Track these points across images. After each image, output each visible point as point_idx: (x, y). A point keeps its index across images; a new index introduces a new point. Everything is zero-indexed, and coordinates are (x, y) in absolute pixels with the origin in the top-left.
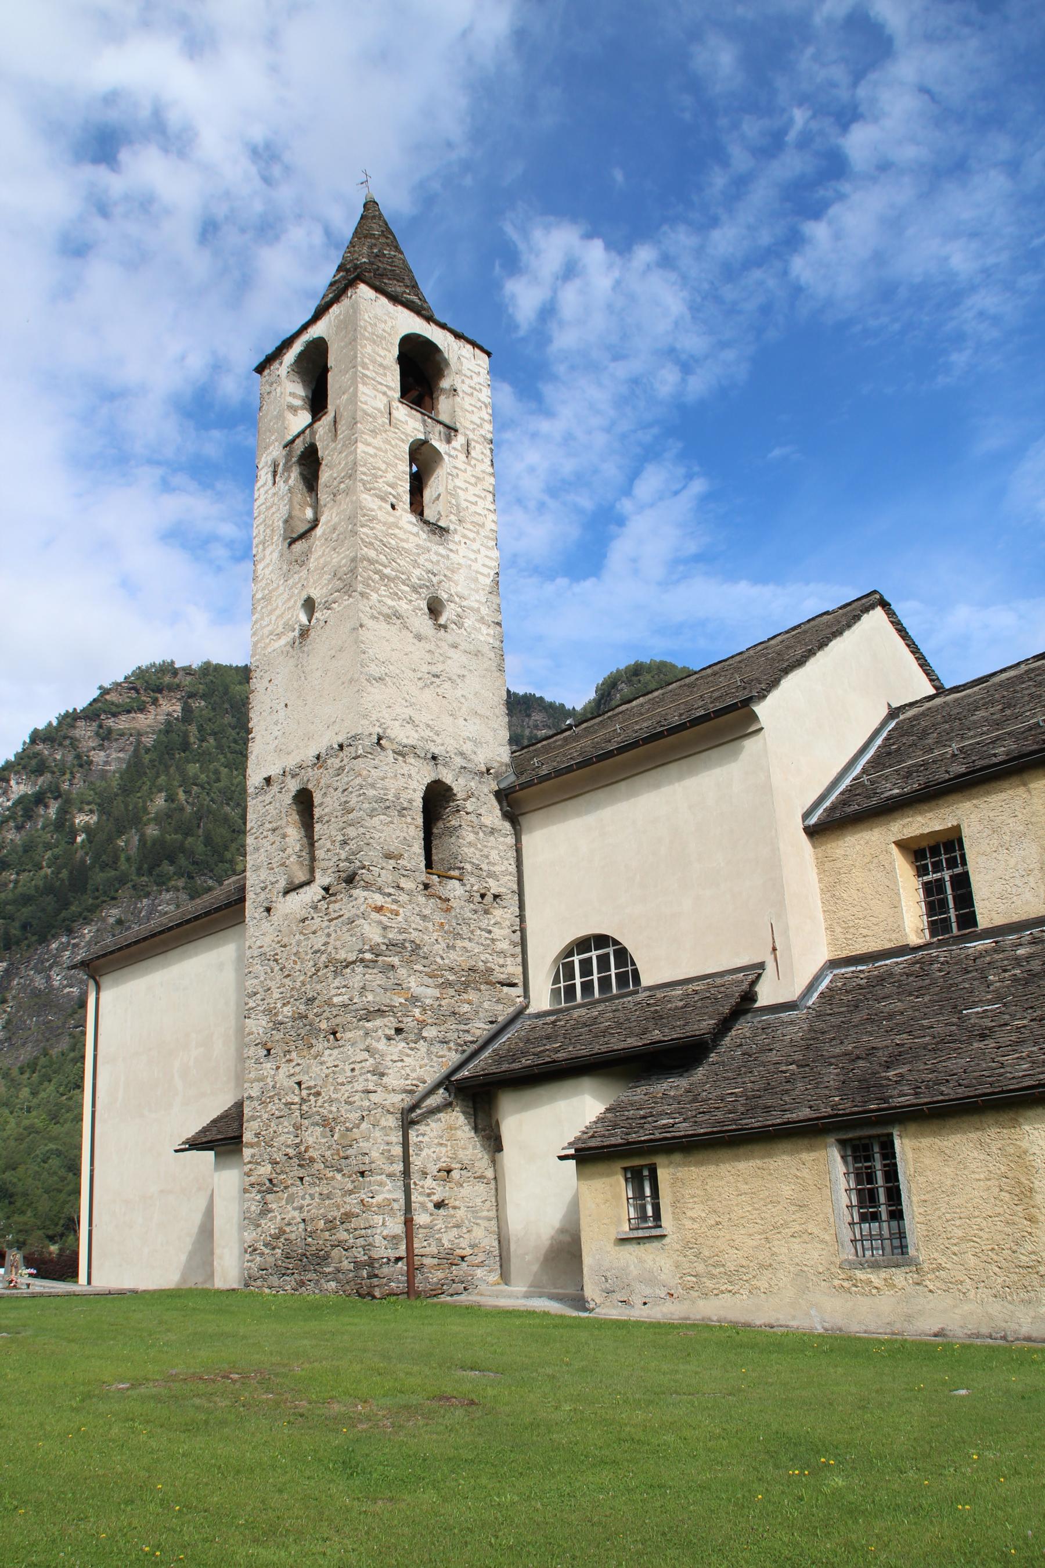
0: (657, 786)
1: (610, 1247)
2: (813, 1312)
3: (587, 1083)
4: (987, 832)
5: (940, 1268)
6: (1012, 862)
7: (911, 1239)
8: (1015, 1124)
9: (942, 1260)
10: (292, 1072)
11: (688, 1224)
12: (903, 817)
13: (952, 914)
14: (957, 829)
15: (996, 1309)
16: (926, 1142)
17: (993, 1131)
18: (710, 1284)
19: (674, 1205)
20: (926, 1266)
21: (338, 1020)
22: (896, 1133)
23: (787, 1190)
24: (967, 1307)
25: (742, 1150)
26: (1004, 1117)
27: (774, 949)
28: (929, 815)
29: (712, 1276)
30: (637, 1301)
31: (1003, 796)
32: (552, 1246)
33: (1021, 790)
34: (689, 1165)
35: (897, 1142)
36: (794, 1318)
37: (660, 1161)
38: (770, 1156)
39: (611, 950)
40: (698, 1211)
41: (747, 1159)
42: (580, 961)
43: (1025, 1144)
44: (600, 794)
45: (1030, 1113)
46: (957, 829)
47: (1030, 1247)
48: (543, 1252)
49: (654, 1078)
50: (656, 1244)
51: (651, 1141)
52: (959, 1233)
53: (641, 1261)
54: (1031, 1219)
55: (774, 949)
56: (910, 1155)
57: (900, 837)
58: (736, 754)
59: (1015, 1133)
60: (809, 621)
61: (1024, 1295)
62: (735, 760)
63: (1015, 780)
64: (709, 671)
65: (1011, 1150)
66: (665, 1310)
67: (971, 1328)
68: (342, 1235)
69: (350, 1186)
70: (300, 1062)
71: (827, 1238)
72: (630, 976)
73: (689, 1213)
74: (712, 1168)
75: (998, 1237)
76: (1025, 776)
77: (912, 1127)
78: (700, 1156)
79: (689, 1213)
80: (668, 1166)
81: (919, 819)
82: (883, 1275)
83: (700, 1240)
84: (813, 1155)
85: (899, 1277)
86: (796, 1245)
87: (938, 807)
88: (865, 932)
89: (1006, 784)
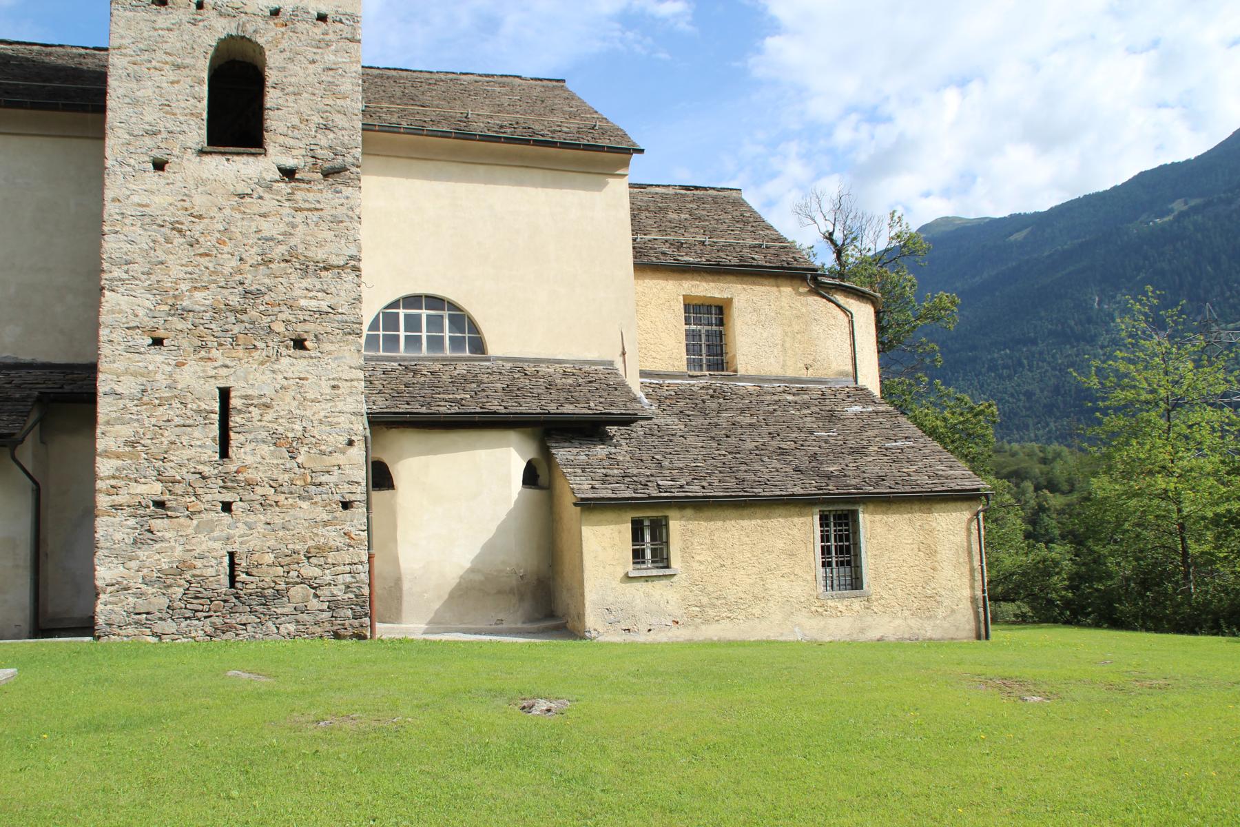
0: (521, 183)
1: (616, 584)
2: (796, 629)
3: (513, 436)
4: (750, 309)
5: (882, 598)
6: (765, 335)
7: (866, 579)
8: (930, 512)
9: (883, 593)
10: (213, 373)
11: (695, 565)
12: (692, 279)
13: (424, 334)
14: (729, 301)
15: (913, 622)
16: (878, 517)
17: (917, 515)
18: (712, 613)
19: (683, 550)
20: (873, 597)
21: (308, 327)
22: (860, 510)
23: (780, 544)
24: (898, 622)
25: (745, 512)
26: (924, 507)
27: (624, 354)
28: (712, 284)
29: (714, 606)
30: (643, 628)
31: (763, 289)
32: (459, 584)
33: (775, 289)
34: (701, 519)
35: (861, 516)
36: (782, 634)
37: (671, 513)
38: (768, 517)
39: (402, 312)
40: (705, 556)
41: (750, 518)
42: (406, 316)
43: (934, 524)
44: (455, 168)
45: (938, 506)
46: (729, 301)
47: (933, 585)
48: (449, 589)
49: (576, 443)
50: (664, 582)
51: (667, 497)
52: (894, 576)
53: (647, 595)
54: (934, 569)
55: (624, 354)
56: (868, 525)
57: (688, 292)
58: (600, 187)
59: (930, 517)
60: (502, 76)
61: (927, 614)
62: (600, 190)
63: (772, 281)
64: (394, 73)
65: (927, 527)
66: (670, 634)
67: (899, 635)
68: (309, 571)
69: (325, 517)
70: (228, 362)
71: (809, 578)
72: (478, 345)
73: (697, 558)
74: (720, 523)
75: (915, 579)
76: (779, 282)
77: (871, 507)
78: (708, 513)
79: (697, 558)
80: (680, 519)
81: (704, 284)
82: (845, 603)
83: (705, 579)
84: (802, 519)
85: (857, 605)
86: (784, 583)
87: (719, 281)
88: (654, 355)
89: (766, 282)
